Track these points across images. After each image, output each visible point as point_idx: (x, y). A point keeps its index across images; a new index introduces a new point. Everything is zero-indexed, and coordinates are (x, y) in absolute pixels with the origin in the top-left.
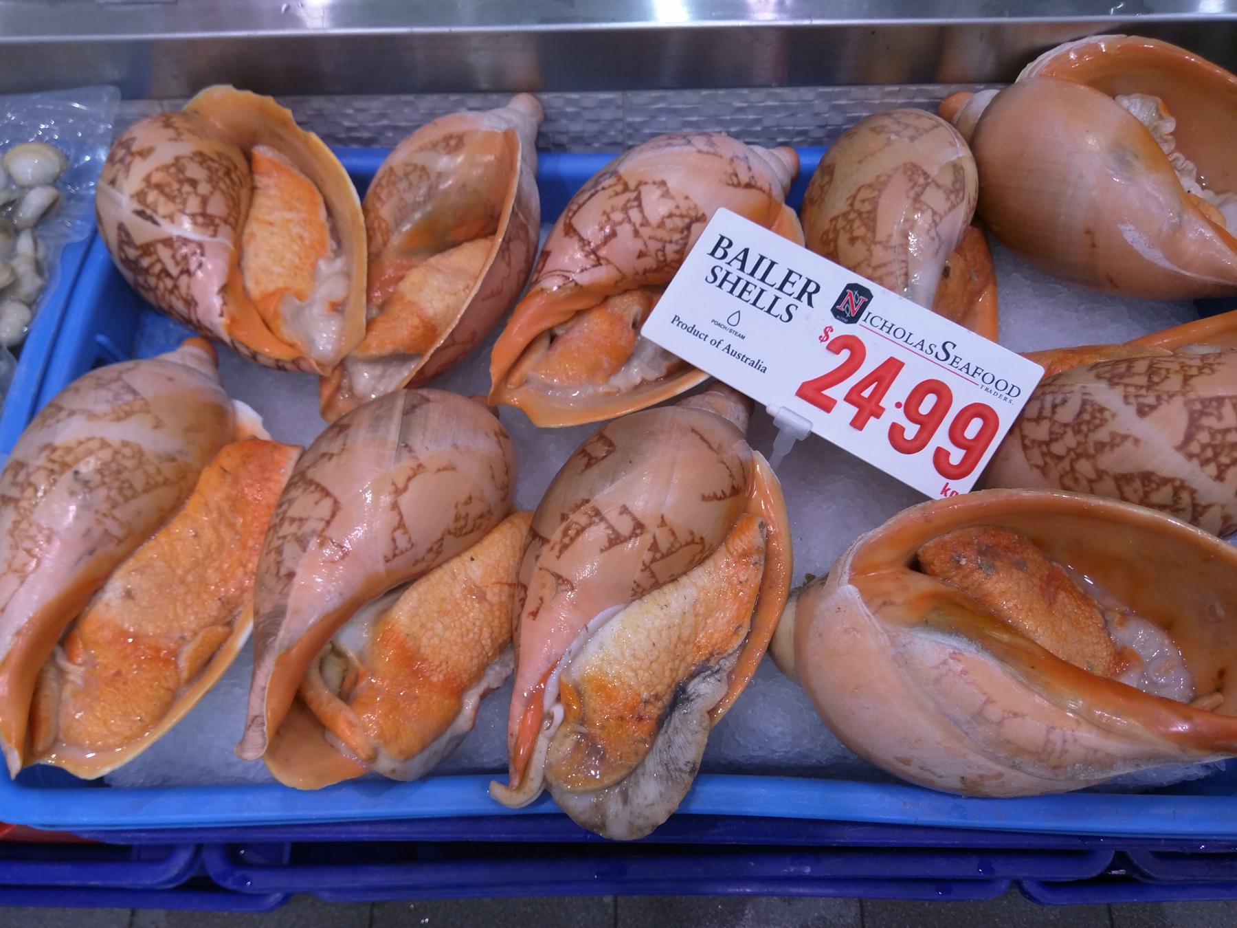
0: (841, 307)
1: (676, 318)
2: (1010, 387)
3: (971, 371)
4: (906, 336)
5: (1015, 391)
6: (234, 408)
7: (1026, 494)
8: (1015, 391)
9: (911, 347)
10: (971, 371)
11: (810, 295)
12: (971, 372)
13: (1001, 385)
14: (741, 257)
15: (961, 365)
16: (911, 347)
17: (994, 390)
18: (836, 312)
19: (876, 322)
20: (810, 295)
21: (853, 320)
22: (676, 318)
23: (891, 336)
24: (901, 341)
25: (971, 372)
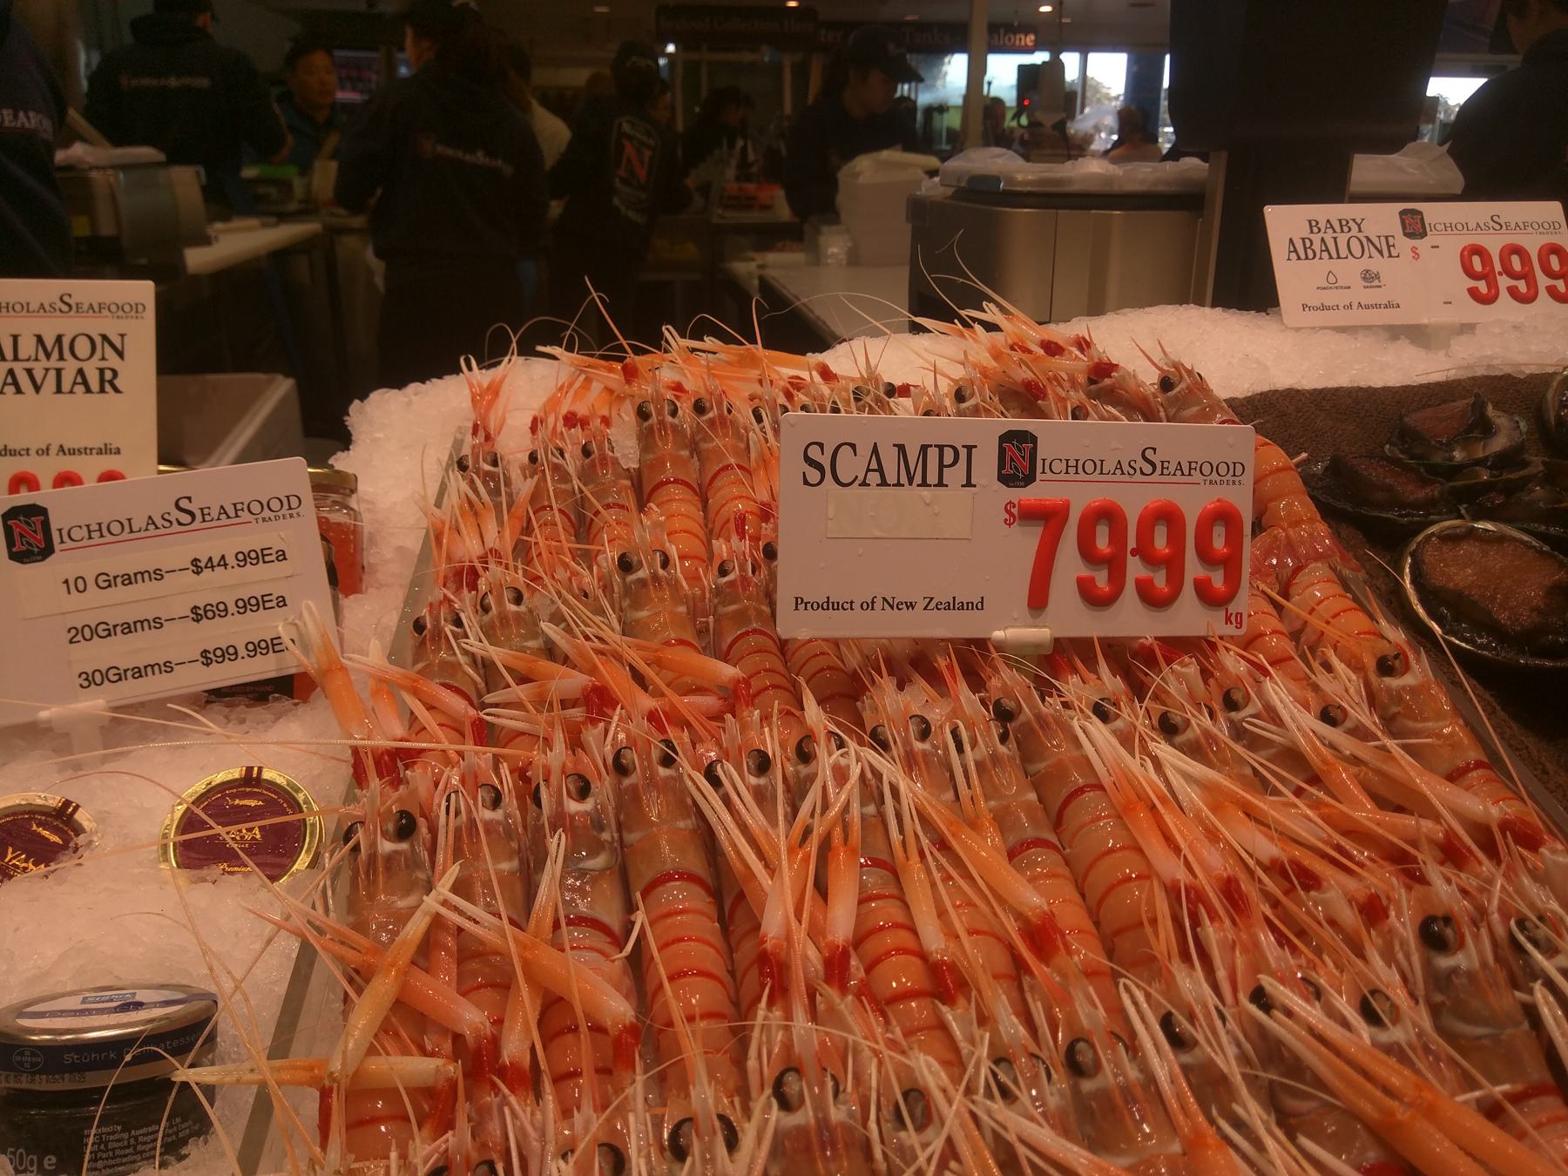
0: (1007, 471)
1: (1304, 306)
2: (126, 524)
3: (231, 513)
4: (1099, 466)
5: (1239, 468)
6: (1474, 72)
7: (83, 58)
8: (1239, 468)
9: (215, 523)
10: (231, 513)
11: (111, 383)
12: (232, 514)
13: (275, 505)
14: (874, 465)
15: (215, 514)
16: (215, 523)
17: (1218, 479)
18: (1006, 479)
19: (1057, 466)
20: (111, 383)
21: (1029, 479)
22: (1304, 306)
23: (109, 538)
24: (126, 535)
25: (232, 514)
